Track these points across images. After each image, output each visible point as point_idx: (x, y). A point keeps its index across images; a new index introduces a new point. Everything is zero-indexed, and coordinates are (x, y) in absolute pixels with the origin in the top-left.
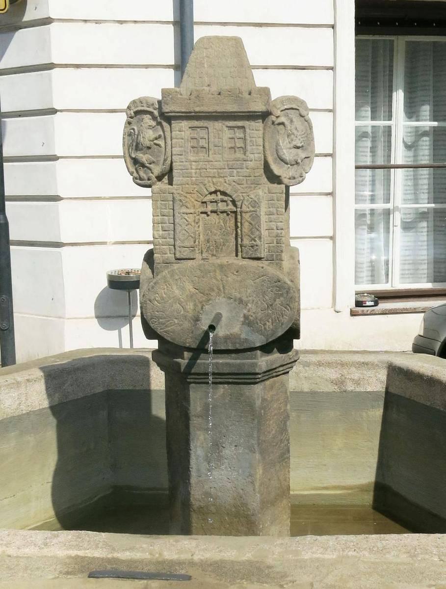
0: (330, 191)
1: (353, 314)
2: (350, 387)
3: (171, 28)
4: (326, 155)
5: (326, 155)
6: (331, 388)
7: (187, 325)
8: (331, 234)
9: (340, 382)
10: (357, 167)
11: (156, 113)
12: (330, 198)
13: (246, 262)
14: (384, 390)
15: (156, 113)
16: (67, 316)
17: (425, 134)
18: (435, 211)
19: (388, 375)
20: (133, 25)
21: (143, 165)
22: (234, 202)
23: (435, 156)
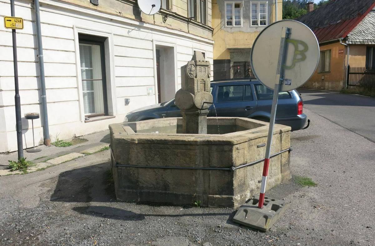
0: (76, 87)
1: (85, 122)
2: (171, 124)
3: (32, 37)
4: (74, 77)
5: (74, 77)
6: (169, 125)
7: (200, 104)
8: (78, 99)
9: (170, 124)
10: (82, 80)
11: (195, 65)
12: (76, 89)
13: (206, 92)
14: (176, 124)
15: (195, 65)
16: (7, 131)
17: (84, 71)
18: (88, 93)
19: (177, 121)
20: (21, 34)
21: (192, 74)
22: (204, 81)
23: (87, 78)
